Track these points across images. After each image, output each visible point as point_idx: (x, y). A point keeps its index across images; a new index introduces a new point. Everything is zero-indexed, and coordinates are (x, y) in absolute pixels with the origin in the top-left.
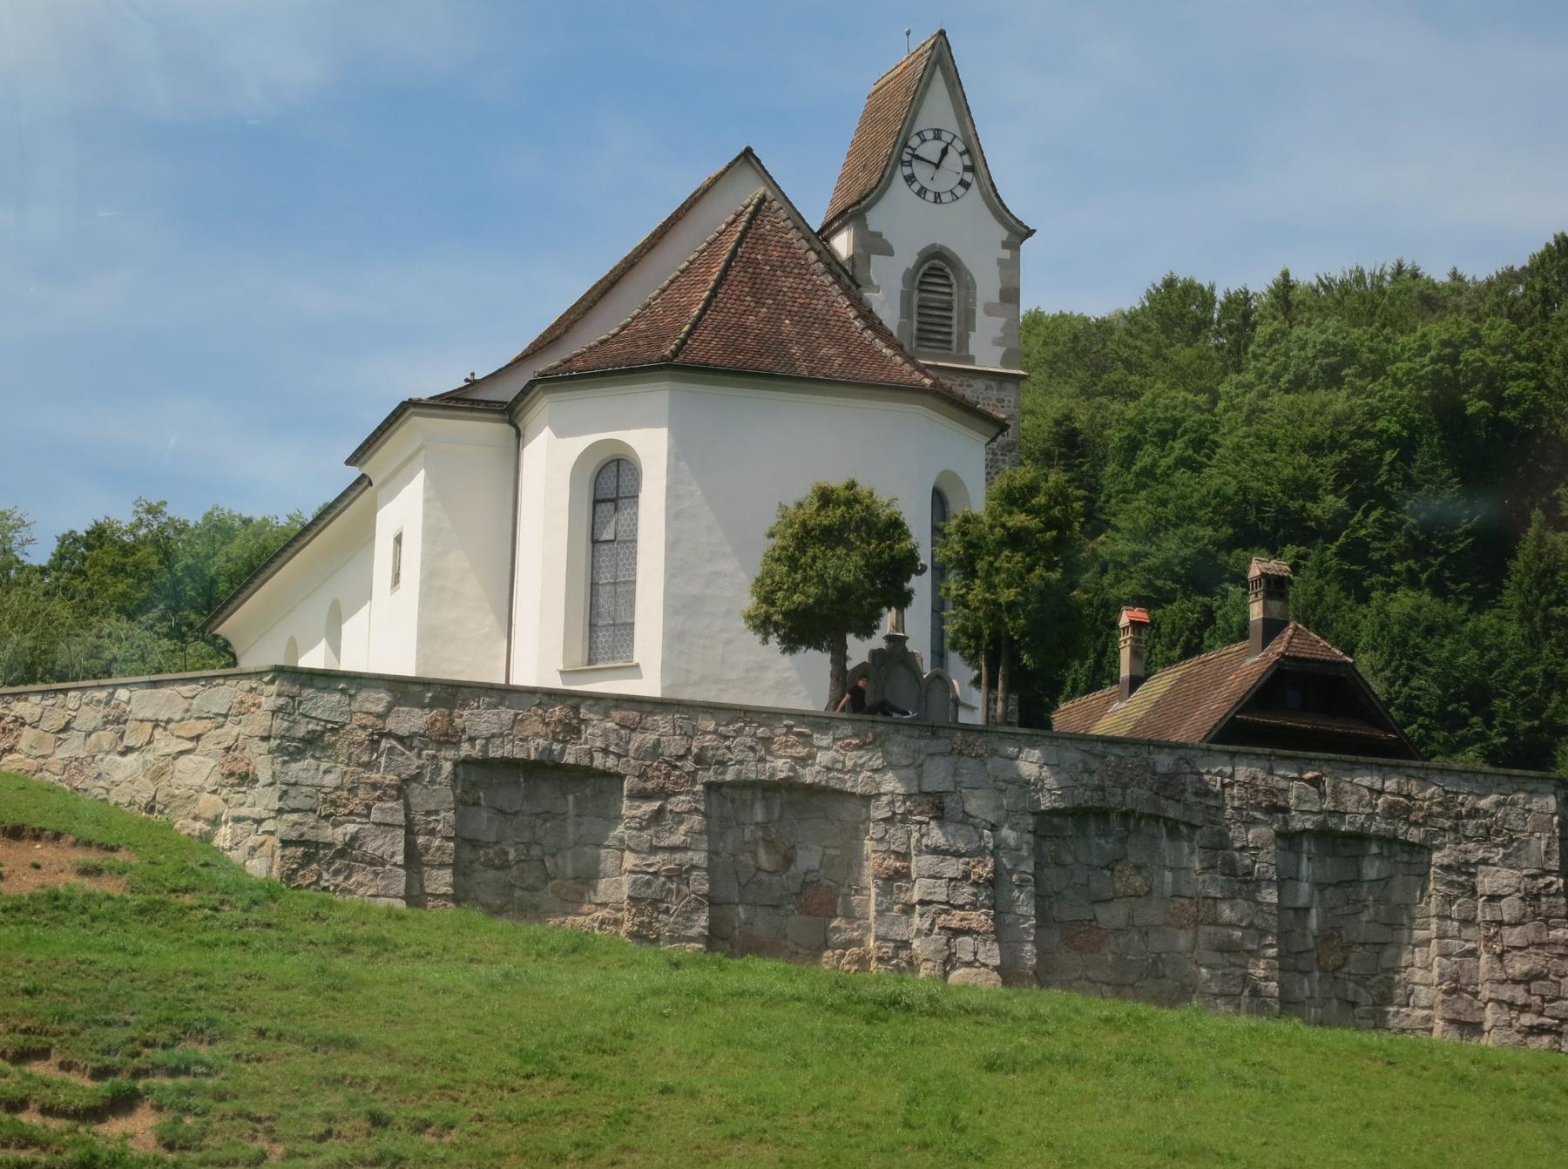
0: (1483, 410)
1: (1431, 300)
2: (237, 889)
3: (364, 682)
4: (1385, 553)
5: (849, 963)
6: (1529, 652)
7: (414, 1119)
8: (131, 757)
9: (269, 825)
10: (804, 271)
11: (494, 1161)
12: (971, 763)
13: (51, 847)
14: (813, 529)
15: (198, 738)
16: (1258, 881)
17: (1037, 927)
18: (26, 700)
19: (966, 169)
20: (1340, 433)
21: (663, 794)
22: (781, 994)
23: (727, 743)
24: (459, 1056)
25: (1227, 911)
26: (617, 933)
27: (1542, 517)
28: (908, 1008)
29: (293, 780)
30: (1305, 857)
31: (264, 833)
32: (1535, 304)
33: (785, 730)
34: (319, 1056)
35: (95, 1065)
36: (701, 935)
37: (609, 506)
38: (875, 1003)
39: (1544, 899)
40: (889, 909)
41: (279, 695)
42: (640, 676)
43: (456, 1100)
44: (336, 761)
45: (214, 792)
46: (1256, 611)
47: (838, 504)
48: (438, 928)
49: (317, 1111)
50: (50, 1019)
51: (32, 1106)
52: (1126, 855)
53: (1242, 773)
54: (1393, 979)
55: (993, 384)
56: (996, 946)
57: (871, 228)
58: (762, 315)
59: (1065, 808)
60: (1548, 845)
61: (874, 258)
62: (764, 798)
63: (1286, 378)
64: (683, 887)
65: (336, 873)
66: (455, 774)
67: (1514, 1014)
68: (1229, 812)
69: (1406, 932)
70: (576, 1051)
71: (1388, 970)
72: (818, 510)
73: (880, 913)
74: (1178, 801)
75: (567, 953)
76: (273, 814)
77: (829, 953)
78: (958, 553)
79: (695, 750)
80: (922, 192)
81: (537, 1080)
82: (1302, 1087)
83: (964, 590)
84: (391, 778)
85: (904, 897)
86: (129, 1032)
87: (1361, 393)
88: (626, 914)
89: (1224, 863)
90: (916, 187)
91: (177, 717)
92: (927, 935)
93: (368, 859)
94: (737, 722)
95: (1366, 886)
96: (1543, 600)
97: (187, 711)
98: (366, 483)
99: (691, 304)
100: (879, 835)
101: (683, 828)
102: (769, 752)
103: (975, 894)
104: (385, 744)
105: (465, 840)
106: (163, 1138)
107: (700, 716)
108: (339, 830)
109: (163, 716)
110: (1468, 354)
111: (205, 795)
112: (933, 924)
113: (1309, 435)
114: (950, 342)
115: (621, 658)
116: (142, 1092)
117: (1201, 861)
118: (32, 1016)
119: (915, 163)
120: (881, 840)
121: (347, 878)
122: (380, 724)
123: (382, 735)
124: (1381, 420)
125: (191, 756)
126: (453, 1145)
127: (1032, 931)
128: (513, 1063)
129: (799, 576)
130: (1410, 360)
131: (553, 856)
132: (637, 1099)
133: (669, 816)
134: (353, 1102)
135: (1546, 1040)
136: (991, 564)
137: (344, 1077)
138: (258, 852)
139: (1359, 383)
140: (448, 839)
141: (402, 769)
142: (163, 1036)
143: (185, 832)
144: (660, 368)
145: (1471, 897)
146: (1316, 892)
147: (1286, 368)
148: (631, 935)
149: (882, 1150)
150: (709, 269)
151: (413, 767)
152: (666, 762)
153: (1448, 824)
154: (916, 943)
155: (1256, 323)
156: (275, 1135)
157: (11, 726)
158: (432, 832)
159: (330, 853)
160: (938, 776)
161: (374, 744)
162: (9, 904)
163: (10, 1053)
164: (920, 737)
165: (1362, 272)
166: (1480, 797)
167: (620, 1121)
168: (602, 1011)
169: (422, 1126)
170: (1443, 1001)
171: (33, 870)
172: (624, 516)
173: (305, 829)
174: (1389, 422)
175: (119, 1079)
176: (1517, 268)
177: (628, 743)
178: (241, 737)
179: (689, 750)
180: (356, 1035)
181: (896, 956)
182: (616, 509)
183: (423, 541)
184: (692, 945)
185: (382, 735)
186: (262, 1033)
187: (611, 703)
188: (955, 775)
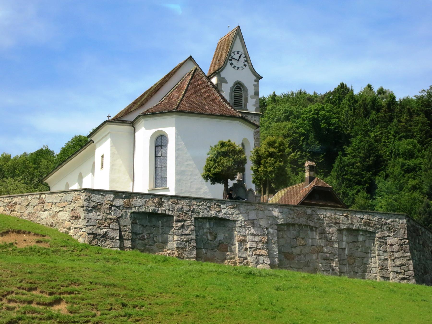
0: (325, 126)
1: (311, 99)
2: (77, 246)
3: (107, 192)
4: (302, 163)
5: (231, 263)
6: (339, 187)
7: (133, 304)
8: (46, 212)
9: (84, 229)
10: (207, 87)
11: (155, 315)
12: (261, 212)
13: (28, 235)
14: (220, 152)
15: (64, 207)
16: (333, 241)
17: (278, 254)
18: (17, 198)
19: (245, 61)
20: (290, 132)
21: (184, 220)
22: (222, 271)
23: (200, 207)
24: (143, 288)
25: (326, 249)
26: (173, 257)
27: (341, 153)
28: (254, 274)
29: (90, 218)
30: (344, 235)
31: (83, 231)
32: (336, 100)
33: (214, 204)
34: (107, 289)
35: (49, 292)
36: (195, 257)
37: (160, 147)
38: (245, 273)
39: (404, 245)
40: (241, 250)
41: (86, 196)
42: (169, 191)
43: (143, 300)
44: (101, 213)
45: (69, 221)
46: (307, 175)
47: (226, 146)
48: (129, 256)
49: (108, 303)
50: (36, 280)
51: (34, 302)
52: (300, 235)
53: (328, 214)
54: (367, 266)
55: (253, 116)
56: (269, 259)
57: (222, 76)
58: (197, 98)
59: (284, 224)
60: (404, 232)
61: (223, 84)
62: (209, 222)
63: (275, 119)
64: (190, 244)
65: (102, 242)
66: (131, 216)
67: (397, 275)
68: (325, 224)
69: (370, 254)
70: (172, 286)
71: (366, 264)
72: (221, 147)
73: (239, 251)
74: (313, 221)
75: (162, 262)
76: (85, 227)
77: (226, 261)
78: (255, 158)
79: (191, 209)
80: (234, 67)
81: (164, 294)
82: (354, 293)
83: (257, 168)
84: (115, 217)
85: (245, 247)
86: (57, 283)
87: (294, 123)
88: (175, 252)
89: (325, 237)
90: (233, 66)
91: (58, 202)
92: (251, 256)
93: (110, 238)
94: (202, 202)
95: (359, 243)
96: (342, 174)
97: (61, 200)
98: (92, 142)
99: (179, 95)
100: (238, 231)
101: (189, 229)
102: (210, 210)
103: (263, 246)
104: (113, 208)
105: (134, 233)
106: (69, 310)
107: (193, 200)
108: (102, 231)
109: (55, 201)
110: (322, 113)
111: (66, 222)
112: (253, 253)
113: (282, 133)
114: (242, 105)
115: (164, 186)
116: (62, 298)
117: (319, 237)
118: (32, 279)
119: (232, 60)
120: (239, 232)
121: (104, 243)
122: (112, 203)
123: (112, 206)
124: (300, 129)
125: (62, 212)
126: (144, 311)
127: (277, 255)
128: (157, 290)
129: (216, 165)
130: (307, 114)
131: (156, 237)
132: (190, 299)
133: (185, 226)
134: (117, 300)
135: (406, 281)
136: (265, 161)
137: (114, 294)
138: (81, 237)
139: (294, 120)
140: (129, 232)
141: (118, 215)
142: (66, 284)
143: (61, 231)
144: (173, 112)
145: (386, 245)
146: (347, 245)
147: (275, 116)
148: (177, 257)
149: (255, 311)
150: (183, 87)
151: (120, 214)
152: (184, 212)
153: (379, 227)
154: (248, 258)
155: (267, 105)
156: (98, 309)
157: (13, 205)
158: (126, 231)
159: (100, 236)
160: (252, 215)
161: (110, 208)
162: (20, 250)
163: (27, 289)
164: (248, 205)
165: (293, 92)
166: (387, 220)
167: (186, 304)
168: (177, 276)
169: (135, 306)
170: (380, 272)
171: (24, 242)
172: (163, 150)
173: (93, 230)
174: (302, 129)
175: (56, 295)
176: (332, 91)
177: (174, 208)
178: (76, 207)
179: (190, 209)
180: (116, 283)
181: (243, 261)
182: (161, 148)
183: (110, 157)
184: (192, 259)
185: (112, 206)
186: (91, 283)
187: (170, 197)
188: (257, 215)
